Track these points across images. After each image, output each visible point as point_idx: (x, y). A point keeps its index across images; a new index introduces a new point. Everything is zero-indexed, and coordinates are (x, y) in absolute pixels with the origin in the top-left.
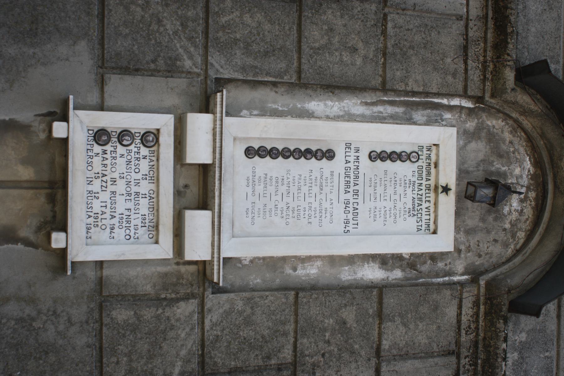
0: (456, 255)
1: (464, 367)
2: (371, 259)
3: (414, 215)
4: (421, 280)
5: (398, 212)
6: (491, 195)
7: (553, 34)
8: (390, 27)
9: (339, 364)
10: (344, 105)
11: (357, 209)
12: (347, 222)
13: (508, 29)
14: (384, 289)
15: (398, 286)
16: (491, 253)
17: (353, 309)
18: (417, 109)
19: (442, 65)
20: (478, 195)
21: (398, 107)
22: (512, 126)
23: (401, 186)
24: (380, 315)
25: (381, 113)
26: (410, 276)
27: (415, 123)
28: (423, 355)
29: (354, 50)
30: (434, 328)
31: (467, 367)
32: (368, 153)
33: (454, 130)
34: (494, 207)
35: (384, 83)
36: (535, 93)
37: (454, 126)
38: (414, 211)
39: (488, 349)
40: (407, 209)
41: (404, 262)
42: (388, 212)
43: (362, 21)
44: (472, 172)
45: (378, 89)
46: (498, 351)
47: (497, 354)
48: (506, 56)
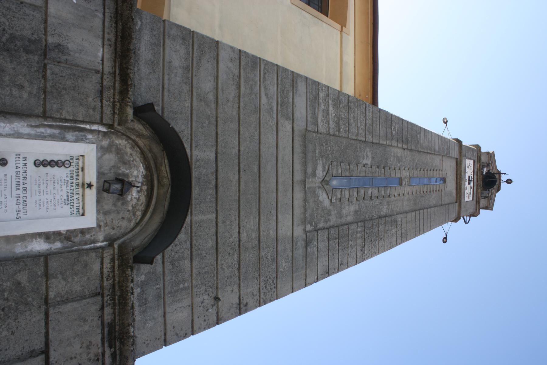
0: (98, 229)
1: (107, 302)
2: (38, 236)
3: (68, 204)
4: (75, 248)
5: (57, 202)
6: (120, 189)
7: (156, 88)
8: (49, 73)
9: (17, 314)
10: (14, 126)
11: (26, 201)
12: (18, 211)
13: (129, 82)
14: (49, 256)
15: (59, 253)
16: (121, 226)
17: (25, 273)
18: (69, 132)
19: (86, 102)
20: (111, 188)
21: (55, 129)
22: (131, 144)
23: (58, 184)
24: (46, 275)
25: (43, 133)
26: (67, 245)
27: (67, 141)
28: (79, 298)
29: (21, 87)
30: (86, 279)
31: (109, 302)
32: (33, 161)
33: (94, 146)
34: (122, 196)
35: (44, 112)
36: (145, 123)
37: (94, 143)
38: (68, 201)
39: (122, 288)
40: (63, 200)
41: (62, 237)
42: (49, 202)
43: (28, 67)
44: (107, 174)
45: (40, 116)
46: (128, 289)
47: (127, 291)
48: (128, 99)
